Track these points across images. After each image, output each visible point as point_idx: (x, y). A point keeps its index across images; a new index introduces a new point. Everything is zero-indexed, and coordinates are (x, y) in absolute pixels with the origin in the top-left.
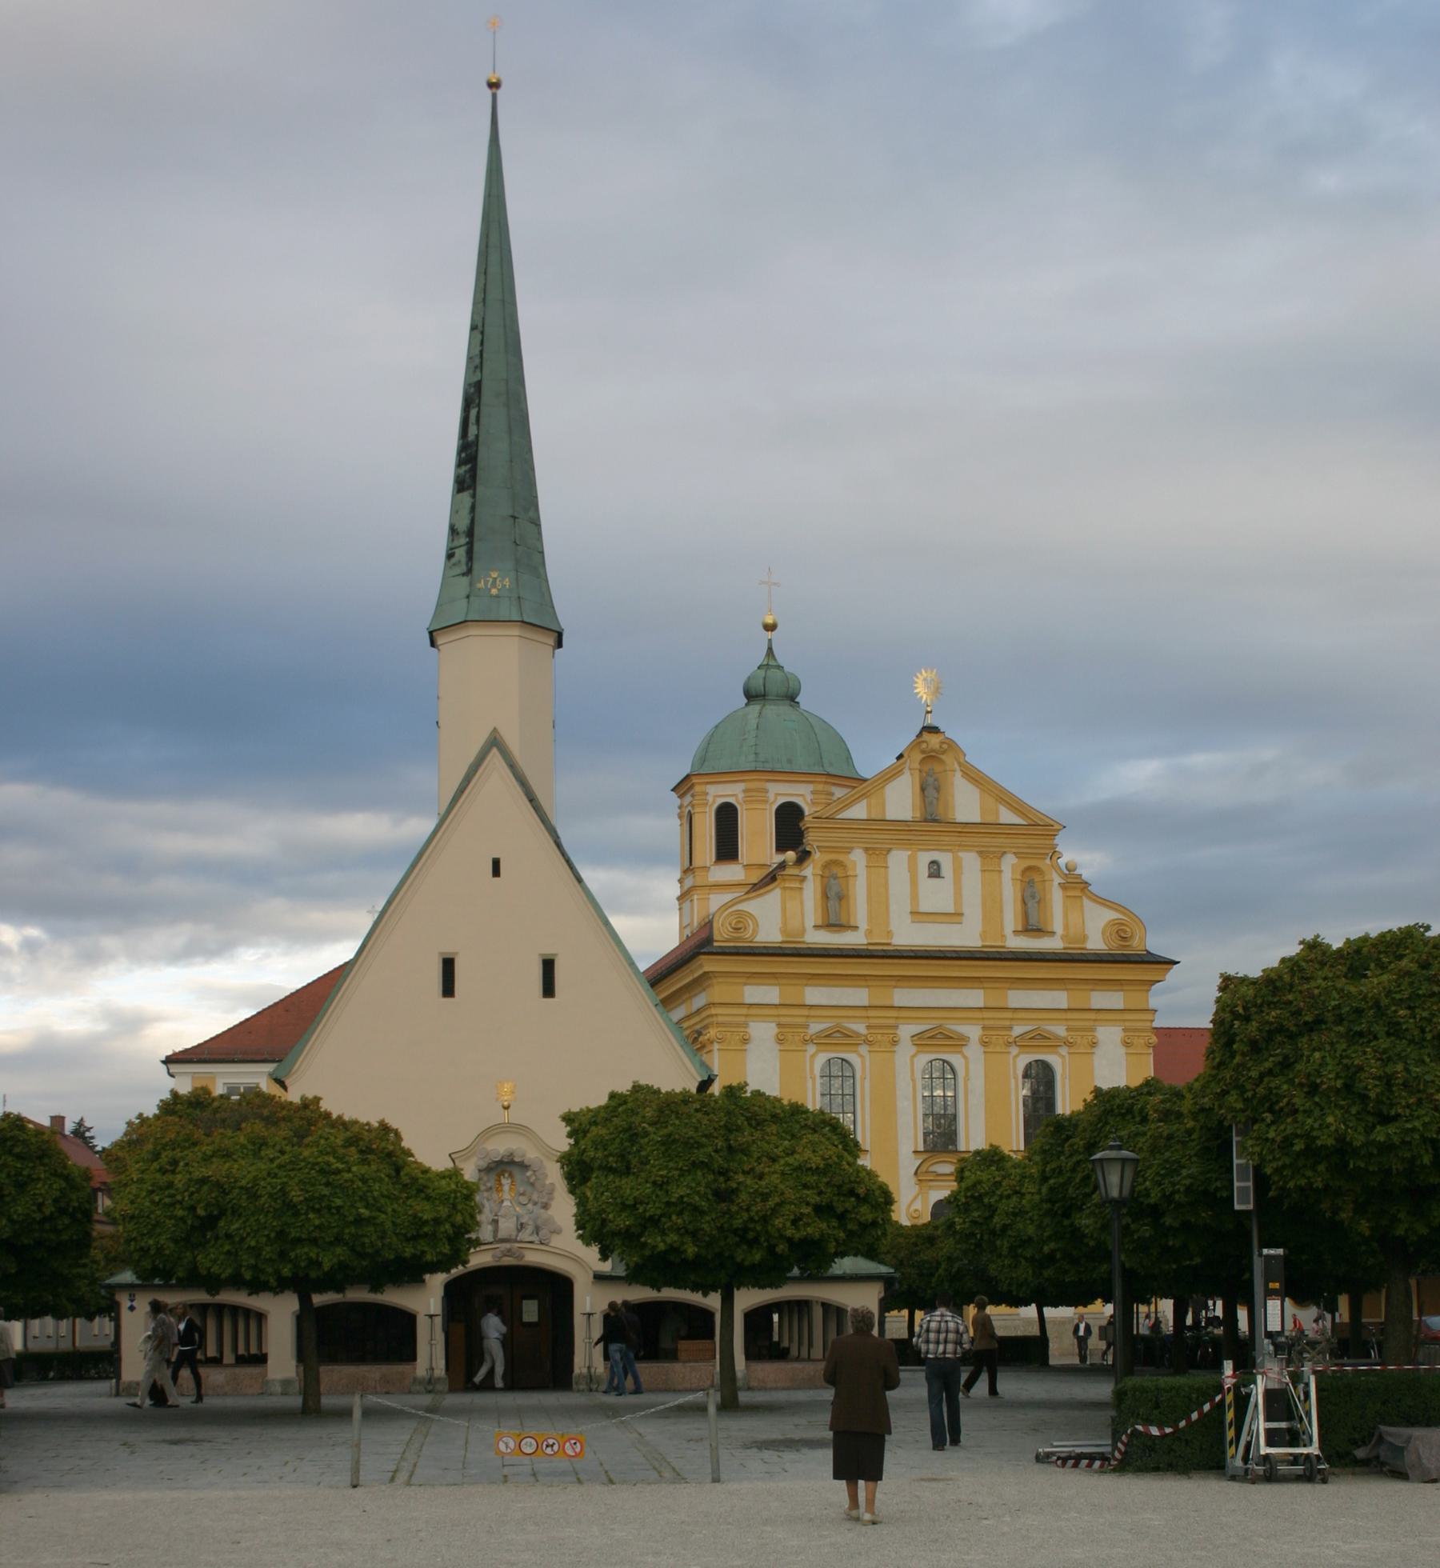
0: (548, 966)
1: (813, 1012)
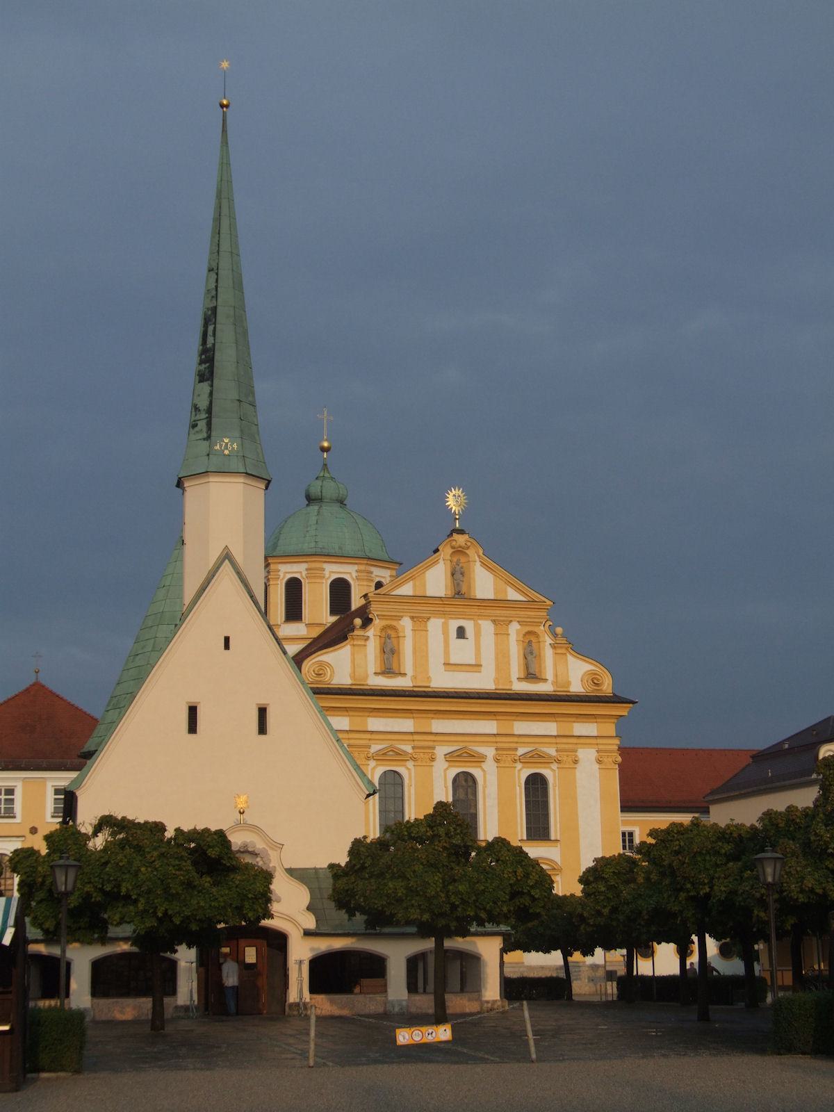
0: (262, 712)
1: (374, 736)
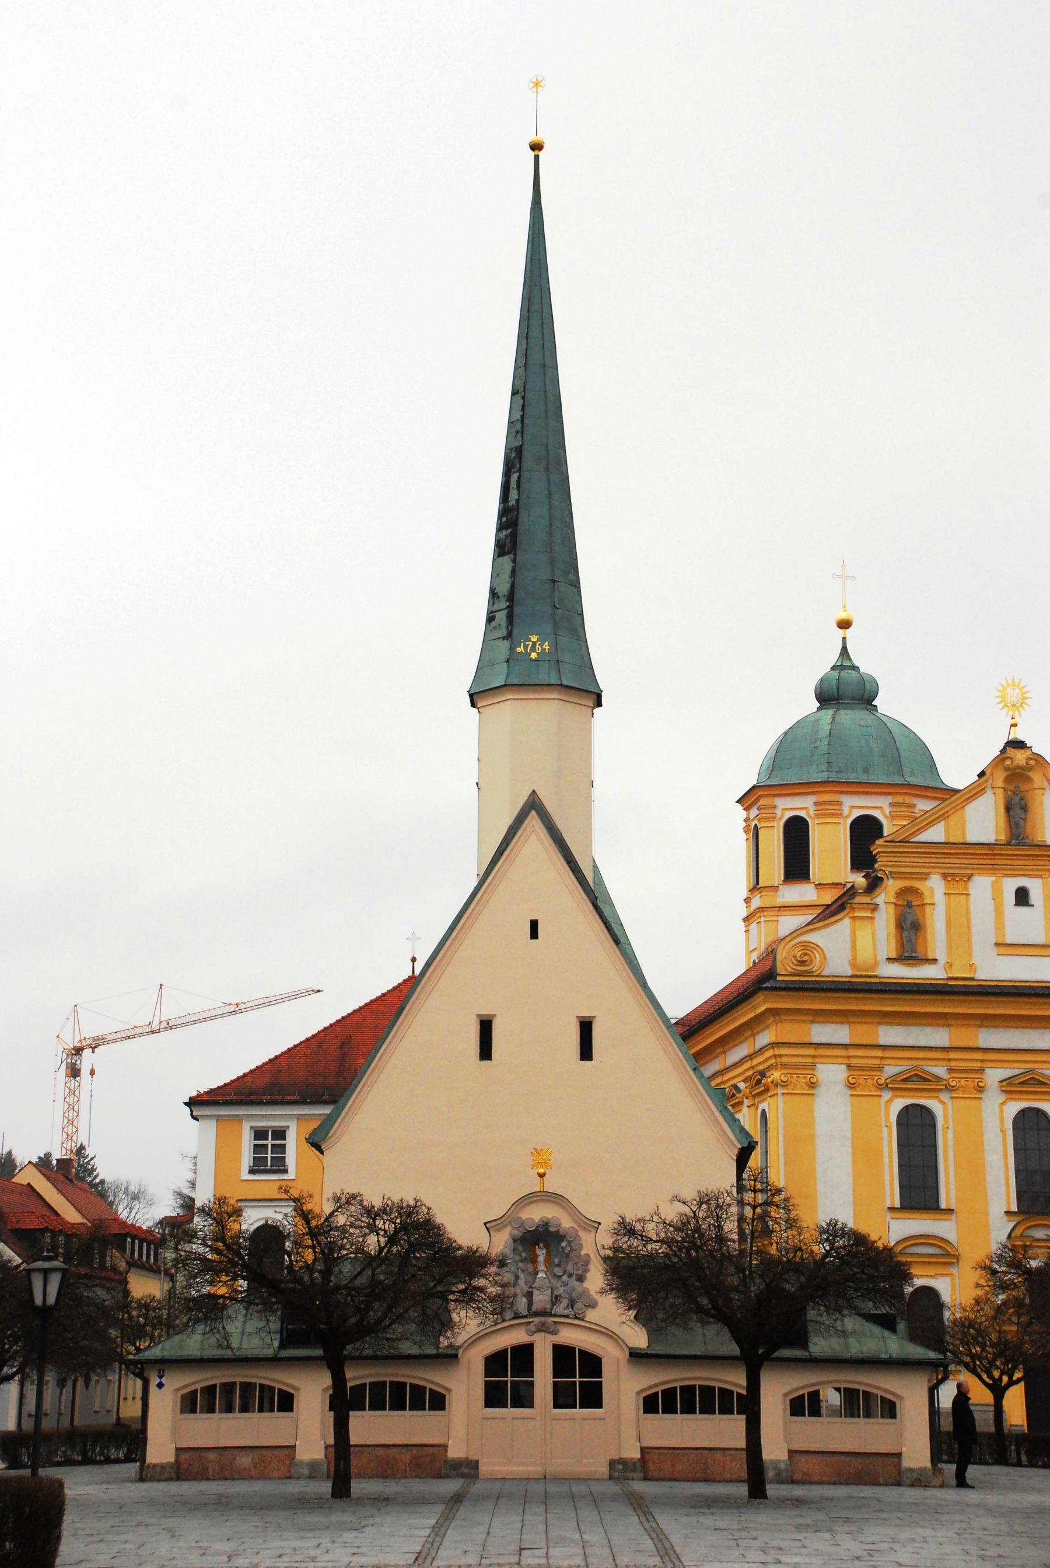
0: (586, 1027)
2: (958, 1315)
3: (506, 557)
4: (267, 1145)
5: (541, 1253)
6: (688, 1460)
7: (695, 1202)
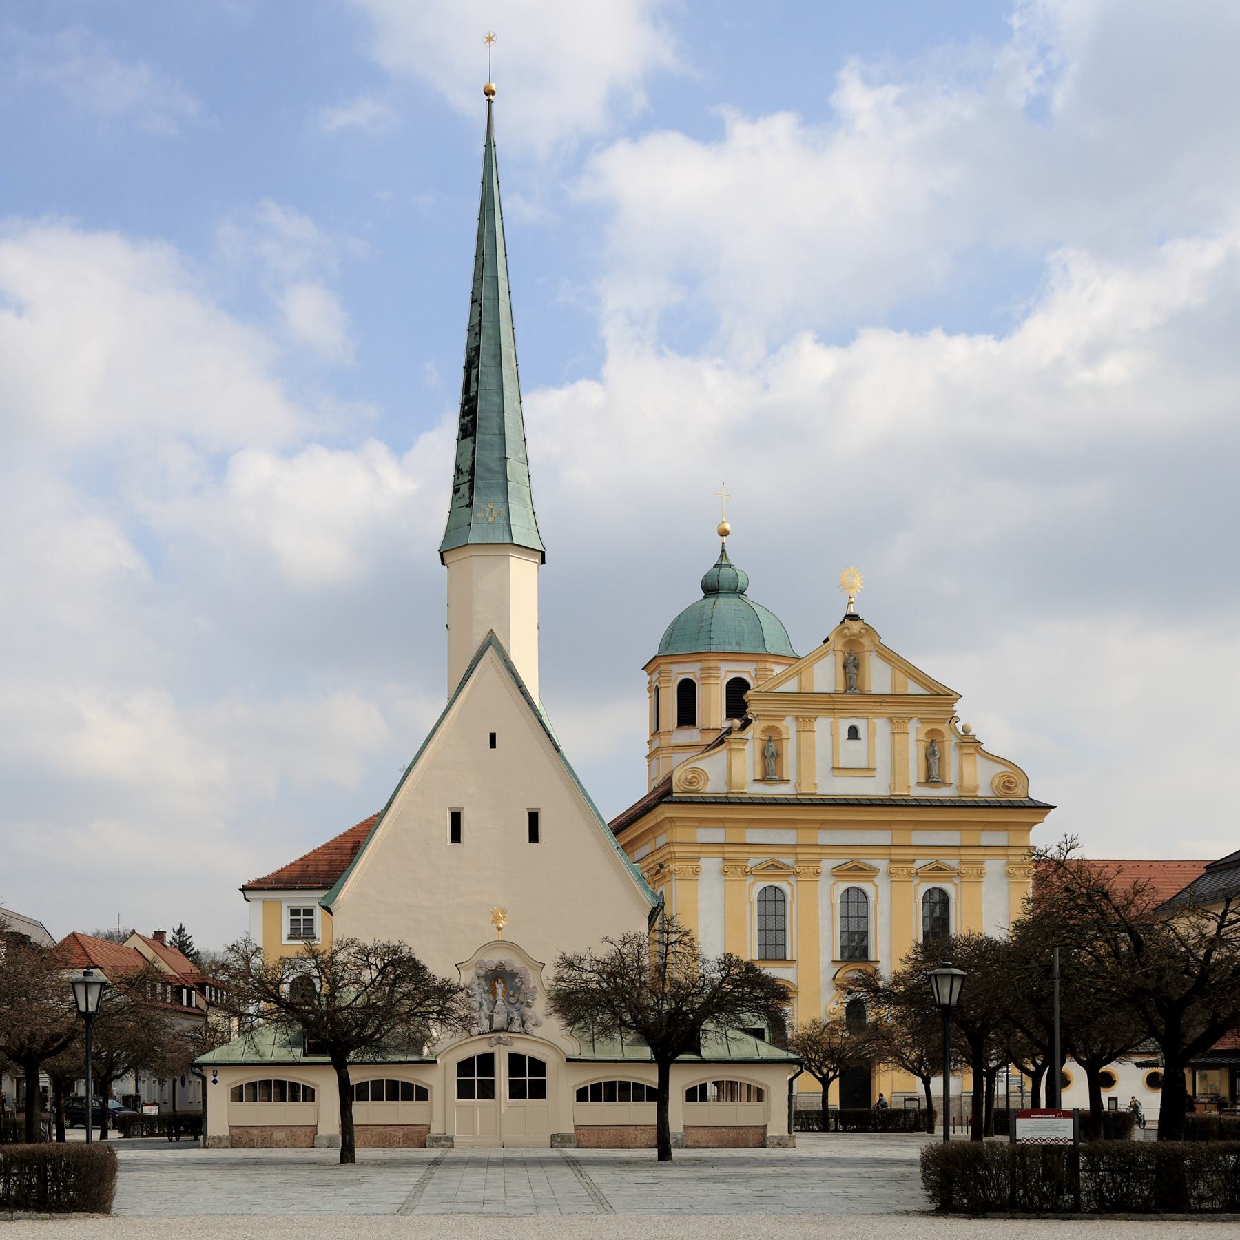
0: (534, 818)
2: (800, 1032)
3: (468, 439)
4: (300, 920)
5: (500, 987)
6: (610, 1134)
7: (621, 942)
